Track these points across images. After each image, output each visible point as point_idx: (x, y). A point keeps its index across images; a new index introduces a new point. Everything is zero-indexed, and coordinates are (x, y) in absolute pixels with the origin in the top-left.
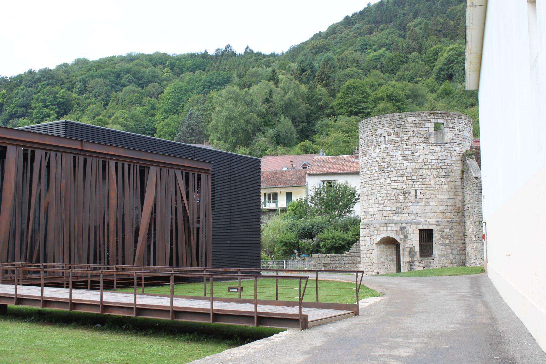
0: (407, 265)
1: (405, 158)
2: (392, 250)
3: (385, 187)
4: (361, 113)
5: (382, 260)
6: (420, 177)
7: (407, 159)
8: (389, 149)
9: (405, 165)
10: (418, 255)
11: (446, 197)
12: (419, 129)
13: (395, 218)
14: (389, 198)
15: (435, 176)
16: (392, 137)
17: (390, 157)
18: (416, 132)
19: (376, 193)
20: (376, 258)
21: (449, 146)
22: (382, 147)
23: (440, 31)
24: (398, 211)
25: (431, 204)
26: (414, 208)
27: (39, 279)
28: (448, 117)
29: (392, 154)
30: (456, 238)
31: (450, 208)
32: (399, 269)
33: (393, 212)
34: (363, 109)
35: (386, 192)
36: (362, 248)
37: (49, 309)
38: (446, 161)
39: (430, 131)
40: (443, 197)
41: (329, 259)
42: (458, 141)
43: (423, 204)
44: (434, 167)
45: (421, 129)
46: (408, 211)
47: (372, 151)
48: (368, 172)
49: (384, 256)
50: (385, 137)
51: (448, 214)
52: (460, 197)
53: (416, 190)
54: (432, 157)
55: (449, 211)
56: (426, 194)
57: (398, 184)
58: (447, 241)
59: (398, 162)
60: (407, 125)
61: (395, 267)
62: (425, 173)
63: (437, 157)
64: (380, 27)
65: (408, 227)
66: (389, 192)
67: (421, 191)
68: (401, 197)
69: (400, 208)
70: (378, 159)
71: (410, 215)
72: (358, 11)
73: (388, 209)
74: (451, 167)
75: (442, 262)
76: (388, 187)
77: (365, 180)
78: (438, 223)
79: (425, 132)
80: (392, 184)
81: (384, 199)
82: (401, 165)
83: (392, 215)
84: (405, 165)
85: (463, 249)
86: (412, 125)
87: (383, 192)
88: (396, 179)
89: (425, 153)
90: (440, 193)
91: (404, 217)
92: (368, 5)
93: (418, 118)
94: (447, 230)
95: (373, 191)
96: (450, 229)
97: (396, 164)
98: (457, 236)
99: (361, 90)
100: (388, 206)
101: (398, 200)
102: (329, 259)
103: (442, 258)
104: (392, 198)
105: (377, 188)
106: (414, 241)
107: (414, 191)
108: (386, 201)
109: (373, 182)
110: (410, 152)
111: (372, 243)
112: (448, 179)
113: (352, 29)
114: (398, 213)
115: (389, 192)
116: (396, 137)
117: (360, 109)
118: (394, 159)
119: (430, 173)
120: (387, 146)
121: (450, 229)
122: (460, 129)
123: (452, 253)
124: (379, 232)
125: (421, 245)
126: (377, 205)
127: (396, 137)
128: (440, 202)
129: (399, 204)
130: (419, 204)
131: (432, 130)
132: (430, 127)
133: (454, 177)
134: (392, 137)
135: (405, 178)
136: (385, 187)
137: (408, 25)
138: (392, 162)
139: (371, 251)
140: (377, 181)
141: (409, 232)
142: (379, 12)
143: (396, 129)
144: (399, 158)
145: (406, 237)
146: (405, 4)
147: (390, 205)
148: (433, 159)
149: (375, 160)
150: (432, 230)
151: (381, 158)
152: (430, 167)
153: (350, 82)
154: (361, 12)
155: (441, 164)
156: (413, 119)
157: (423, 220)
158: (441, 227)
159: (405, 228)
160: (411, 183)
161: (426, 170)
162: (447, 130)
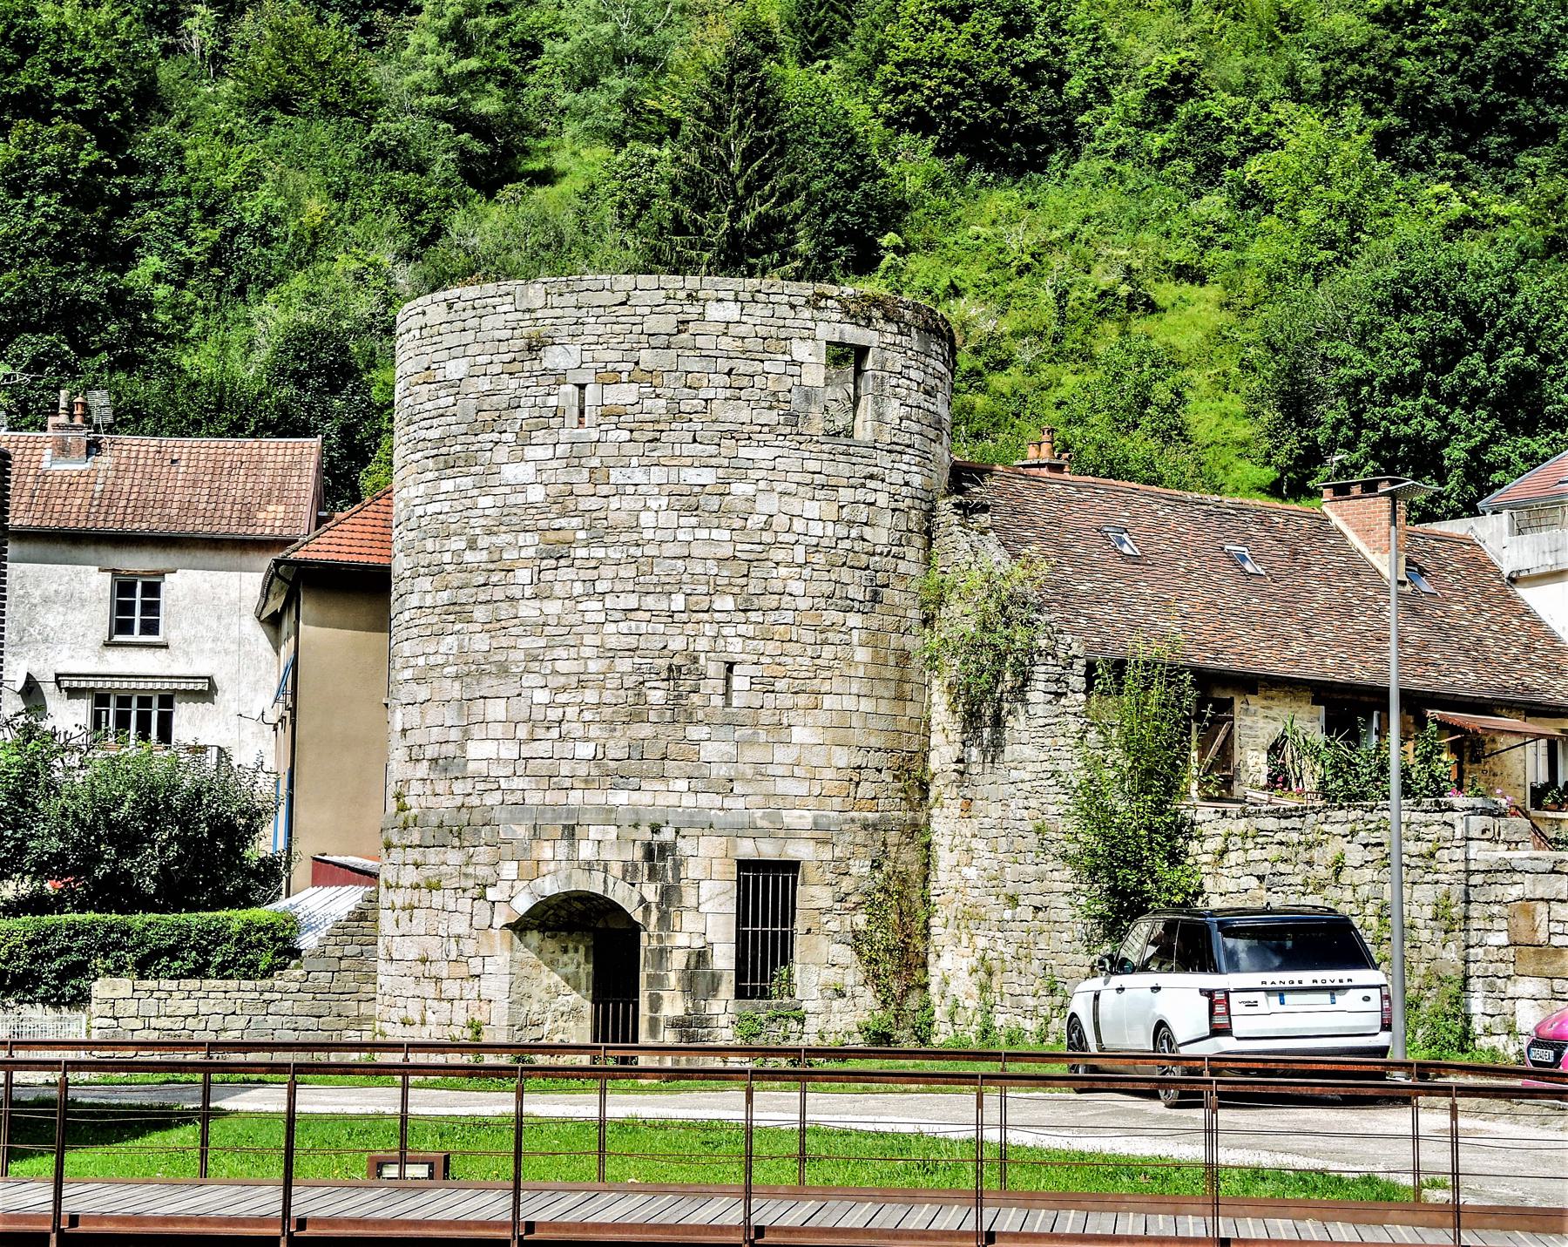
3: (571, 640)
8: (602, 450)
9: (681, 536)
10: (727, 988)
11: (866, 705)
12: (758, 367)
14: (591, 696)
16: (623, 394)
17: (603, 490)
18: (745, 382)
22: (564, 435)
25: (798, 734)
27: (775, 934)
31: (875, 759)
37: (242, 1076)
38: (868, 532)
39: (807, 381)
40: (849, 703)
44: (819, 558)
45: (767, 366)
46: (689, 768)
47: (501, 454)
48: (469, 556)
50: (582, 387)
51: (866, 790)
54: (812, 509)
55: (873, 775)
59: (647, 519)
62: (777, 586)
67: (756, 671)
70: (536, 494)
71: (699, 785)
76: (588, 640)
77: (445, 596)
78: (822, 834)
81: (562, 698)
82: (660, 535)
86: (725, 342)
88: (632, 601)
89: (779, 487)
97: (636, 527)
100: (587, 740)
102: (188, 1007)
104: (608, 697)
105: (525, 643)
106: (709, 921)
108: (571, 712)
109: (505, 610)
110: (708, 477)
111: (481, 920)
115: (593, 666)
118: (629, 503)
119: (796, 587)
128: (841, 725)
134: (623, 394)
135: (678, 602)
139: (476, 966)
140: (528, 610)
141: (692, 870)
144: (653, 504)
145: (669, 895)
149: (520, 499)
150: (793, 866)
151: (552, 490)
155: (847, 544)
156: (731, 311)
160: (710, 630)
161: (783, 571)
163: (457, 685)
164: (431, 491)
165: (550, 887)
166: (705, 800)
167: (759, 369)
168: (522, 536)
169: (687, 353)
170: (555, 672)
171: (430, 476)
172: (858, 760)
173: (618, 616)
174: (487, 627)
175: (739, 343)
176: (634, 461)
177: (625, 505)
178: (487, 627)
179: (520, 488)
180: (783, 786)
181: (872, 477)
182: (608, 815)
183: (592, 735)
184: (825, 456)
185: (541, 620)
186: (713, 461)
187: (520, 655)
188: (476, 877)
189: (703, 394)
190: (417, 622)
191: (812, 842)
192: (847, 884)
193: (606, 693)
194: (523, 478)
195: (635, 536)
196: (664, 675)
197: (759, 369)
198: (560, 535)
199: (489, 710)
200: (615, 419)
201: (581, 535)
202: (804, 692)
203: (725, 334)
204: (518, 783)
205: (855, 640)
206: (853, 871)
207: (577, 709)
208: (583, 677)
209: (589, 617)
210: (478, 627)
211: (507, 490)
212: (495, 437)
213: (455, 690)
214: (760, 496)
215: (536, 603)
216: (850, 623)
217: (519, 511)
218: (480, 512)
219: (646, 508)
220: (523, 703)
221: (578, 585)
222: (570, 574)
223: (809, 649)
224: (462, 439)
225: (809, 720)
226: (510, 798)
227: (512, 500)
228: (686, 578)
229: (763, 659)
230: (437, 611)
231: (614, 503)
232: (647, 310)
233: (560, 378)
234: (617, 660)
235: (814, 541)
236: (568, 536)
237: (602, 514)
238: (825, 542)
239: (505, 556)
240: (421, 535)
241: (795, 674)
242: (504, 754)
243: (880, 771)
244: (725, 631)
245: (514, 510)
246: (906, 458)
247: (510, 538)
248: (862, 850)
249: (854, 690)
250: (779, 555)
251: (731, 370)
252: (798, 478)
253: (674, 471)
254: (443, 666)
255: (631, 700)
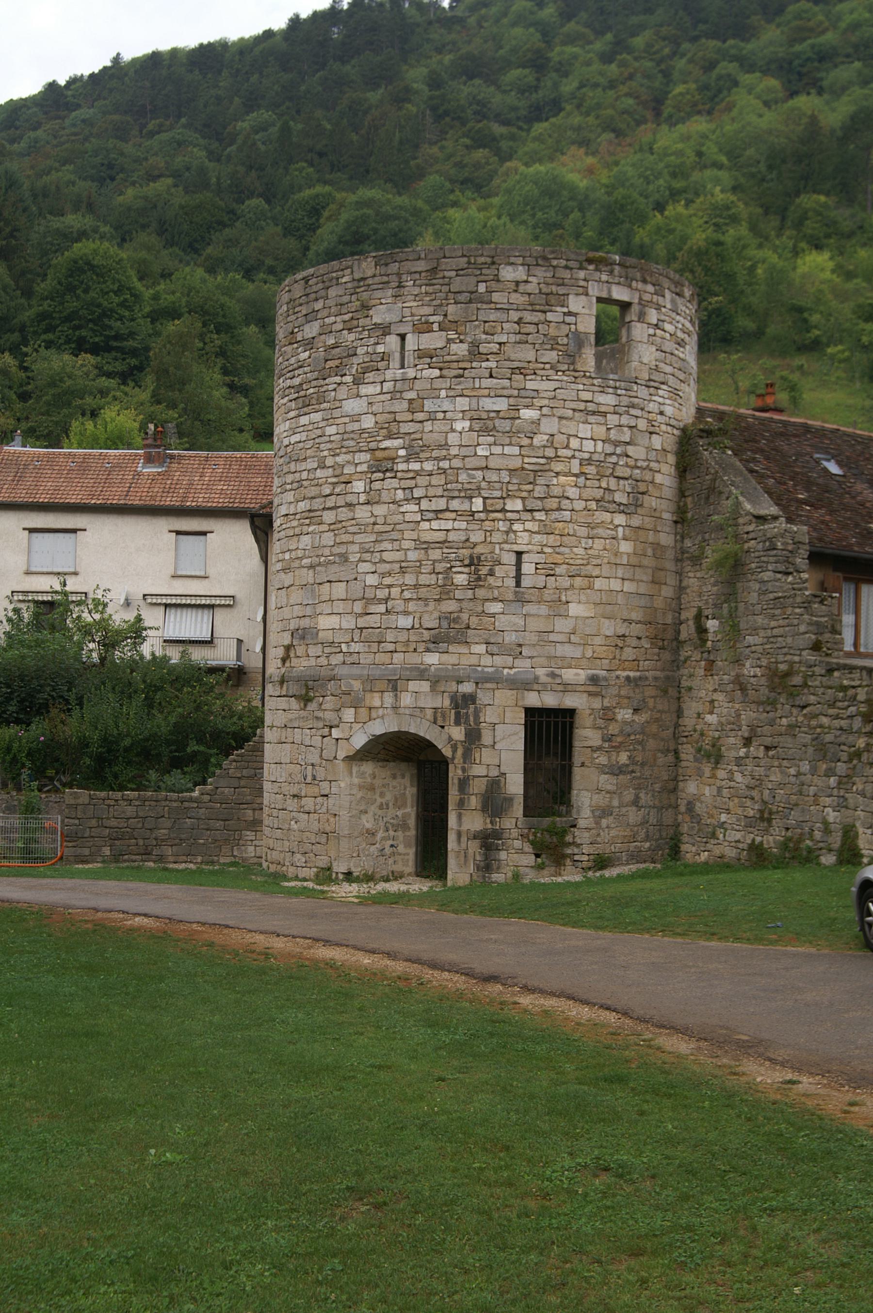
0: (474, 847)
1: (484, 424)
2: (401, 788)
3: (395, 535)
4: (109, 349)
5: (367, 822)
6: (538, 504)
7: (487, 431)
8: (418, 385)
9: (480, 451)
10: (518, 809)
11: (628, 587)
13: (432, 659)
14: (410, 579)
15: (593, 505)
16: (434, 341)
17: (420, 416)
18: (531, 329)
19: (354, 558)
20: (344, 813)
21: (643, 392)
22: (389, 374)
23: (321, 155)
24: (448, 634)
25: (575, 609)
26: (508, 621)
28: (645, 281)
29: (428, 405)
30: (651, 744)
32: (431, 856)
33: (426, 635)
34: (117, 337)
35: (398, 556)
36: (270, 772)
38: (630, 450)
39: (581, 328)
40: (616, 585)
41: (130, 811)
42: (671, 381)
43: (543, 610)
44: (591, 470)
45: (550, 316)
46: (485, 635)
47: (342, 393)
48: (319, 473)
49: (373, 809)
50: (403, 337)
52: (667, 592)
53: (519, 554)
54: (585, 430)
55: (634, 642)
56: (558, 570)
57: (449, 525)
58: (623, 758)
59: (453, 438)
60: (495, 297)
61: (412, 851)
62: (556, 491)
63: (601, 431)
64: (150, 127)
65: (483, 697)
66: (412, 556)
67: (540, 558)
68: (461, 579)
69: (456, 620)
70: (368, 422)
71: (495, 649)
72: (87, 73)
73: (405, 622)
74: (648, 476)
75: (605, 836)
77: (302, 506)
79: (565, 329)
80: (425, 525)
81: (387, 581)
82: (464, 451)
83: (421, 647)
84: (480, 451)
85: (671, 785)
86: (516, 298)
87: (386, 556)
88: (441, 504)
90: (606, 570)
91: (476, 655)
92: (117, 59)
93: (540, 272)
94: (625, 714)
95: (341, 549)
96: (636, 711)
97: (446, 446)
98: (655, 736)
99: (114, 280)
100: (406, 613)
101: (446, 591)
103: (604, 822)
104: (424, 579)
105: (358, 538)
106: (505, 753)
107: (511, 559)
108: (395, 591)
109: (344, 513)
110: (502, 405)
112: (636, 521)
113: (67, 122)
114: (449, 640)
115: (412, 556)
116: (449, 341)
117: (108, 338)
118: (439, 426)
119: (572, 492)
120: (411, 373)
121: (636, 711)
122: (680, 334)
123: (636, 802)
124: (363, 711)
125: (528, 770)
126: (358, 607)
127: (449, 341)
128: (605, 605)
129: (450, 606)
130: (529, 608)
131: (588, 325)
132: (584, 313)
133: (654, 514)
134: (434, 341)
136: (395, 535)
137: (229, 129)
138: (428, 438)
139: (325, 787)
140: (362, 513)
141: (489, 716)
142: (147, 84)
143: (451, 309)
144: (458, 426)
145: (473, 736)
146: (220, 72)
147: (412, 606)
148: (587, 438)
149: (356, 426)
150: (571, 713)
151: (380, 418)
152: (575, 468)
153: (81, 249)
154: (92, 75)
155: (614, 459)
156: (520, 273)
157: (541, 672)
158: (606, 703)
159: (470, 699)
160: (502, 526)
161: (562, 479)
162: (639, 331)
163: (311, 572)
164: (294, 426)
165: (378, 728)
166: (498, 660)
167: (542, 319)
168: (357, 455)
169: (485, 306)
170: (383, 561)
171: (292, 414)
172: (622, 629)
173: (430, 515)
174: (332, 527)
175: (526, 298)
176: (443, 393)
177: (436, 428)
178: (332, 527)
179: (356, 418)
180: (560, 650)
181: (633, 406)
182: (421, 673)
183: (410, 609)
184: (596, 389)
185: (372, 520)
186: (505, 392)
187: (356, 548)
188: (324, 720)
189: (496, 338)
190: (284, 526)
191: (585, 695)
192: (613, 729)
193: (421, 577)
194: (357, 411)
195: (444, 453)
196: (467, 562)
197: (542, 319)
198: (386, 454)
199: (334, 591)
200: (428, 360)
201: (402, 452)
202: (579, 576)
203: (516, 291)
204: (355, 647)
205: (620, 535)
206: (619, 717)
207: (399, 589)
208: (403, 564)
209: (408, 517)
210: (325, 527)
211: (347, 420)
212: (338, 379)
213: (308, 576)
214: (544, 420)
215: (369, 507)
216: (616, 522)
217: (356, 436)
218: (327, 439)
219: (453, 430)
220: (359, 585)
221: (400, 492)
222: (395, 483)
223: (583, 541)
224: (314, 383)
225: (583, 598)
226: (349, 660)
227: (350, 428)
228: (483, 484)
229: (546, 550)
230: (298, 517)
231: (428, 426)
232: (453, 273)
233: (385, 330)
234: (430, 551)
235: (586, 456)
236: (392, 454)
237: (418, 436)
238: (596, 457)
239: (345, 472)
240: (288, 460)
241: (571, 562)
242: (345, 625)
243: (639, 638)
244: (516, 527)
245: (352, 435)
246: (661, 392)
247: (349, 457)
248: (626, 701)
249: (620, 575)
250: (558, 467)
251: (521, 319)
252: (574, 405)
253: (474, 400)
254: (301, 559)
255: (440, 582)
